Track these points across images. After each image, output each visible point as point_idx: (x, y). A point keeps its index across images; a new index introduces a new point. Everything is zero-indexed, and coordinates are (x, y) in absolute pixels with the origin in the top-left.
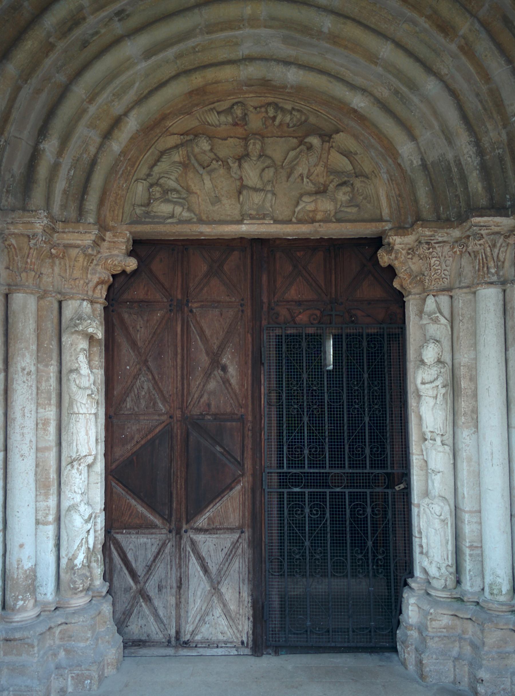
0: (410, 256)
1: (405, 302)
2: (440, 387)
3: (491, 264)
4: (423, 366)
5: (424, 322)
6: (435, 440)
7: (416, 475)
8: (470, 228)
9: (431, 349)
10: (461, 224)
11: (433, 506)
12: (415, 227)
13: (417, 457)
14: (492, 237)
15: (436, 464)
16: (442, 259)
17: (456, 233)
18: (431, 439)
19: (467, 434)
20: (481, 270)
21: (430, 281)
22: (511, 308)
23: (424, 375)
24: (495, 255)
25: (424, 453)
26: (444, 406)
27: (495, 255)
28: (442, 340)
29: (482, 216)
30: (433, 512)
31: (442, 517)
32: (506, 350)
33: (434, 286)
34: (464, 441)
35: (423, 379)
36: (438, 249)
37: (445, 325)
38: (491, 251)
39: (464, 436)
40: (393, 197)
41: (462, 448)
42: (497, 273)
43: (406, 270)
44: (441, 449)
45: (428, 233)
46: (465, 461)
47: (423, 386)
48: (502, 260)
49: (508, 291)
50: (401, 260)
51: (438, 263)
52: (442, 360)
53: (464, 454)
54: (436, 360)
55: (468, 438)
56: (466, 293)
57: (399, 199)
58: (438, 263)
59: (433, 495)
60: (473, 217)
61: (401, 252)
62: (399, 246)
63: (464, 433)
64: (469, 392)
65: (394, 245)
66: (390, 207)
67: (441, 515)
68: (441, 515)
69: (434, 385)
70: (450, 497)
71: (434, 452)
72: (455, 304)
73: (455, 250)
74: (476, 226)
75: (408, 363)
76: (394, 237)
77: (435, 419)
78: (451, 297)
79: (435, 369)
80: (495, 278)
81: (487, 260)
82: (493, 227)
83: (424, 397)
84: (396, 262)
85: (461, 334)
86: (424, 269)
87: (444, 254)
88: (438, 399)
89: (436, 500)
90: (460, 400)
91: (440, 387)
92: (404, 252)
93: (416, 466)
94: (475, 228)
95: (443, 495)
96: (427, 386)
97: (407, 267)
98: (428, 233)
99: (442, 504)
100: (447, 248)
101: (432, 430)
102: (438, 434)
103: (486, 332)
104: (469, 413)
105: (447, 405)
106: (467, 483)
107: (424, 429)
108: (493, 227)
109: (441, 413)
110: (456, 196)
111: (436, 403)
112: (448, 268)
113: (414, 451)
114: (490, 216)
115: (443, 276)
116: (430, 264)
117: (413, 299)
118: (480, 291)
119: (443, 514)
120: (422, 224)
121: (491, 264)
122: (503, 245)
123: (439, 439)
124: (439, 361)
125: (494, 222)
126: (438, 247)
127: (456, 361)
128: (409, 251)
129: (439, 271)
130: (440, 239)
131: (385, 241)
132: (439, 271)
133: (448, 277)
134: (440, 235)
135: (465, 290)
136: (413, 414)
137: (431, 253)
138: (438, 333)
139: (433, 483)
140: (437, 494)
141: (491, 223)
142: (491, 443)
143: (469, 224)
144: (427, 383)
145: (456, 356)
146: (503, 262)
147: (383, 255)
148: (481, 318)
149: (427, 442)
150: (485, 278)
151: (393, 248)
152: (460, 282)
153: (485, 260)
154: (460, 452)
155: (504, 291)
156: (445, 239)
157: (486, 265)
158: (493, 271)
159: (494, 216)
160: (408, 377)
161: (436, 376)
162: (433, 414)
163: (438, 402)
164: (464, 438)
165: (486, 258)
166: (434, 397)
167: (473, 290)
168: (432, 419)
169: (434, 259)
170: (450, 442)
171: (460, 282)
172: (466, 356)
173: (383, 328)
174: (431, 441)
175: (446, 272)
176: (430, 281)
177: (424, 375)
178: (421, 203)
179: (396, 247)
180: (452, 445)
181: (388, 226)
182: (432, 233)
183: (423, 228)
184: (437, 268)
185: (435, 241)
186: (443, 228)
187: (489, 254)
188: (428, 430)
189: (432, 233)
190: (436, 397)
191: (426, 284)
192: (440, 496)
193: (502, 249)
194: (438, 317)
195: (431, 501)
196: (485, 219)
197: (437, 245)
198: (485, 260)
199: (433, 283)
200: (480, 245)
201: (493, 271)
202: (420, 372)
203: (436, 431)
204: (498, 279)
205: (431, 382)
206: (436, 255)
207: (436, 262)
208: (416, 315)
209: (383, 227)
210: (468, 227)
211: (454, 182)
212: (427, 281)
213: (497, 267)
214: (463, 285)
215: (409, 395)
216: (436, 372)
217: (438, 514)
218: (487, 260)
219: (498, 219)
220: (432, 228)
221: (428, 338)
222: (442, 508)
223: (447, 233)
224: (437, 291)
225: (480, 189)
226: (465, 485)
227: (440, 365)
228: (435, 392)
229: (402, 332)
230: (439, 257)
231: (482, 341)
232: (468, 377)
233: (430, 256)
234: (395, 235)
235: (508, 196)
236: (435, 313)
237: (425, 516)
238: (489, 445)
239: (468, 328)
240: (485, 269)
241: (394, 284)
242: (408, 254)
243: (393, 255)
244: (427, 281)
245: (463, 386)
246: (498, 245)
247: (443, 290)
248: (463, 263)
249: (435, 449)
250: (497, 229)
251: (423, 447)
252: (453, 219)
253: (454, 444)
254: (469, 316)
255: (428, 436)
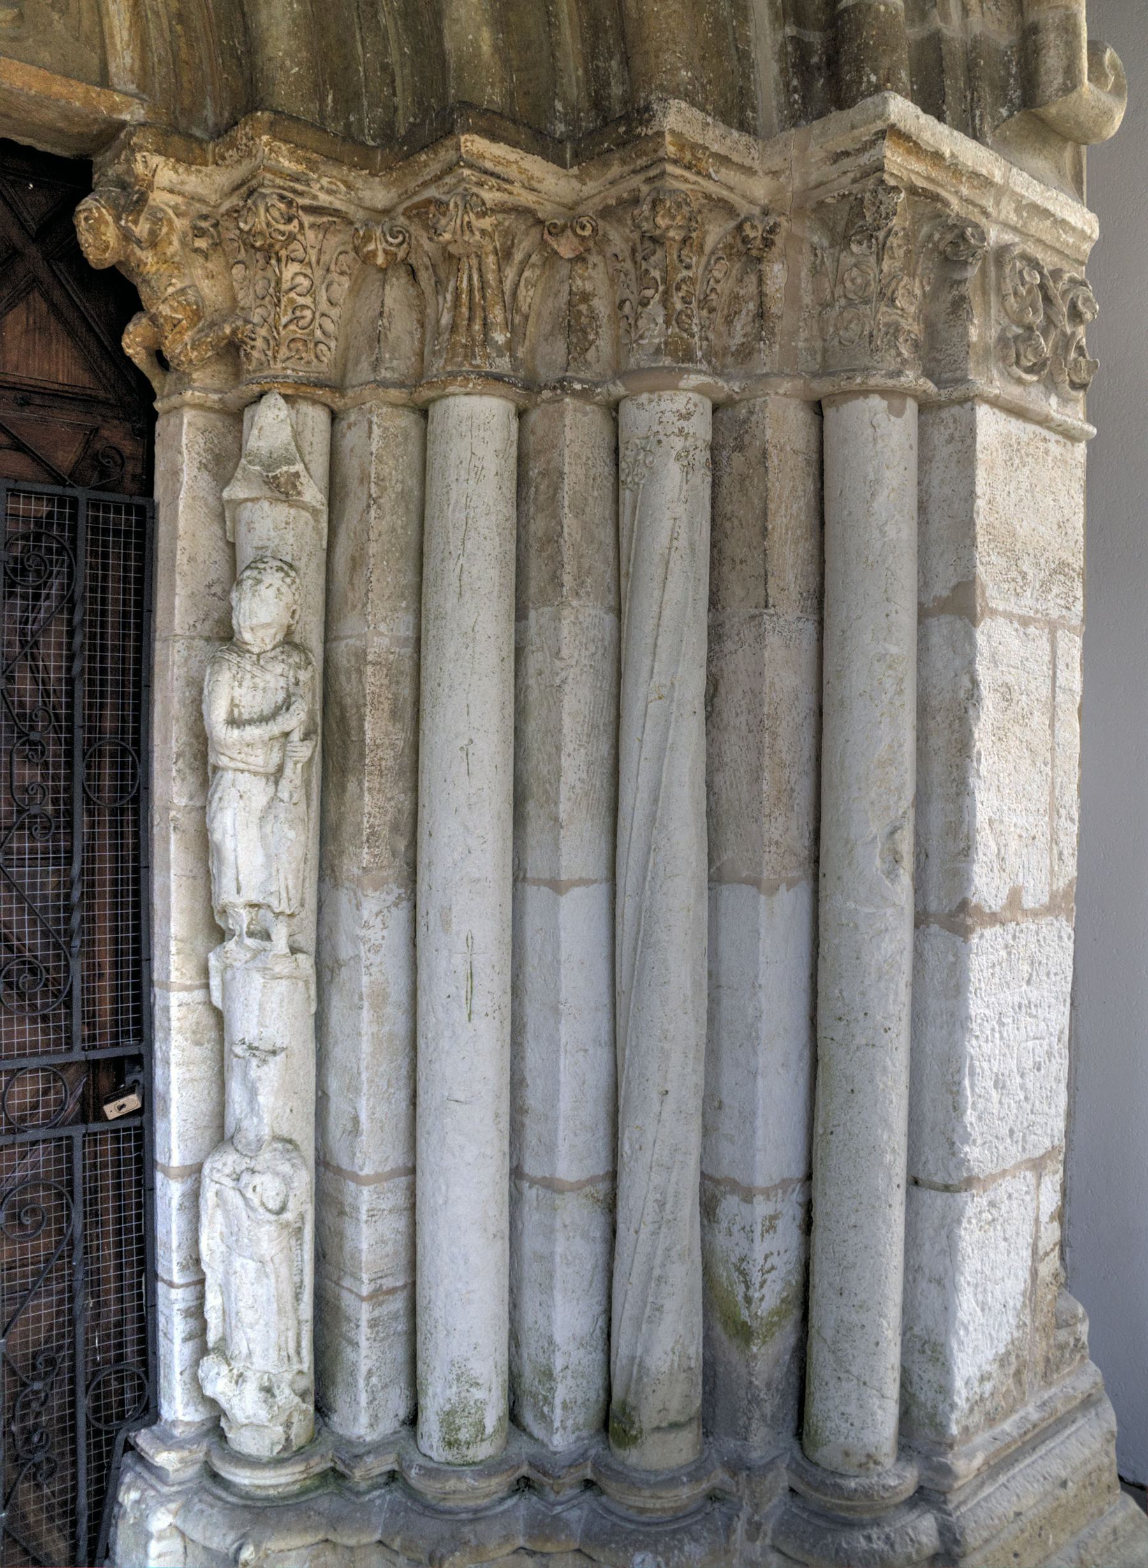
0: (201, 243)
1: (154, 416)
2: (296, 737)
3: (497, 315)
4: (234, 658)
5: (237, 491)
6: (267, 936)
7: (178, 1064)
8: (450, 169)
9: (271, 592)
10: (407, 156)
11: (257, 1180)
12: (241, 133)
13: (184, 996)
14: (509, 221)
15: (261, 1024)
16: (319, 272)
17: (378, 194)
18: (251, 934)
19: (376, 909)
20: (462, 330)
21: (274, 343)
22: (544, 474)
23: (238, 692)
24: (508, 286)
25: (215, 982)
26: (303, 806)
27: (508, 286)
28: (301, 564)
29: (493, 136)
30: (256, 1202)
31: (289, 1216)
32: (520, 613)
33: (286, 367)
34: (362, 933)
35: (233, 704)
36: (310, 234)
37: (315, 512)
38: (499, 270)
39: (366, 914)
40: (157, 14)
41: (357, 957)
42: (510, 346)
43: (183, 291)
44: (283, 967)
45: (287, 164)
46: (366, 1004)
47: (236, 732)
48: (525, 309)
49: (534, 416)
50: (170, 251)
51: (306, 283)
52: (297, 639)
53: (365, 979)
54: (280, 637)
55: (378, 922)
56: (394, 405)
57: (179, 28)
58: (306, 283)
59: (251, 1136)
60: (469, 130)
61: (170, 221)
62: (167, 196)
63: (365, 905)
64: (388, 758)
65: (150, 186)
66: (143, 45)
67: (283, 1209)
68: (283, 1209)
69: (275, 728)
70: (305, 1136)
71: (258, 980)
72: (352, 438)
73: (371, 247)
74: (471, 166)
75: (158, 645)
76: (156, 160)
77: (268, 856)
78: (334, 417)
79: (279, 668)
80: (503, 364)
81: (484, 297)
82: (516, 188)
83: (229, 776)
84: (148, 257)
85: (373, 548)
86: (245, 298)
87: (325, 258)
88: (284, 783)
89: (266, 1156)
90: (352, 786)
91: (296, 737)
92: (180, 224)
93: (180, 1031)
94: (466, 172)
95: (285, 1132)
96: (253, 732)
97: (187, 283)
98: (287, 164)
99: (286, 1168)
100: (333, 242)
101: (255, 897)
102: (278, 915)
103: (469, 545)
104: (385, 832)
105: (308, 806)
106: (371, 1081)
107: (227, 894)
108: (516, 188)
109: (292, 834)
110: (385, 67)
111: (275, 799)
112: (334, 312)
113: (174, 976)
114: (514, 144)
115: (318, 333)
116: (278, 282)
117: (195, 406)
118: (451, 401)
119: (290, 1205)
120: (272, 124)
121: (497, 315)
122: (535, 258)
123: (280, 935)
124: (289, 642)
125: (522, 171)
126: (312, 226)
127: (342, 649)
128: (204, 224)
129: (308, 313)
130: (324, 199)
131: (109, 170)
132: (308, 313)
133: (333, 344)
134: (325, 181)
135: (394, 394)
136: (173, 837)
137: (292, 237)
138: (290, 538)
139: (253, 1092)
140: (266, 1132)
141: (512, 172)
142: (469, 940)
143: (446, 155)
144: (250, 722)
145: (350, 626)
146: (526, 318)
147: (100, 220)
148: (453, 495)
149: (231, 945)
150: (474, 356)
151: (143, 199)
152: (376, 366)
153: (477, 296)
154: (344, 973)
155: (521, 414)
156: (338, 205)
157: (479, 313)
158: (500, 337)
159: (528, 151)
160: (158, 697)
161: (281, 696)
162: (263, 838)
163: (284, 795)
164: (366, 925)
165: (482, 289)
166: (267, 776)
167: (426, 393)
168: (259, 859)
169: (294, 267)
170: (307, 939)
171: (376, 366)
172: (383, 628)
173: (74, 503)
174: (249, 942)
175: (330, 327)
176: (274, 343)
177: (238, 692)
178: (270, 51)
179: (158, 198)
180: (312, 949)
181: (133, 113)
182: (301, 168)
183: (275, 137)
184: (301, 300)
185: (306, 201)
186: (338, 161)
187: (491, 277)
188: (240, 900)
189: (301, 168)
190: (277, 775)
191: (255, 354)
192: (277, 1138)
193: (527, 274)
194: (297, 475)
195: (245, 1163)
196: (499, 150)
197: (307, 219)
198: (477, 296)
199: (284, 352)
200: (483, 232)
201: (500, 337)
202: (225, 677)
203: (274, 903)
204: (515, 369)
205: (264, 719)
206: (300, 254)
207: (300, 279)
208: (203, 466)
209: (114, 108)
210: (435, 168)
211: (383, 19)
212: (259, 343)
213: (509, 325)
214: (385, 374)
215: (157, 766)
216: (282, 682)
217: (274, 1205)
218: (484, 297)
219: (535, 166)
220: (303, 147)
221: (247, 553)
222: (287, 1181)
223: (349, 187)
224: (298, 383)
225: (486, 48)
226: (365, 1087)
227: (296, 658)
228: (275, 757)
229: (141, 524)
230: (310, 264)
231: (453, 577)
232: (386, 706)
233: (283, 253)
234: (158, 151)
235: (559, 106)
236: (290, 462)
237: (219, 1216)
238: (461, 946)
239: (394, 530)
240: (477, 327)
241: (126, 341)
242: (200, 233)
243: (142, 229)
244: (259, 343)
245: (369, 735)
246: (518, 256)
247: (318, 384)
248: (389, 302)
249: (264, 970)
250: (526, 198)
251: (213, 962)
252: (371, 143)
253: (319, 942)
254: (399, 487)
255: (242, 919)
